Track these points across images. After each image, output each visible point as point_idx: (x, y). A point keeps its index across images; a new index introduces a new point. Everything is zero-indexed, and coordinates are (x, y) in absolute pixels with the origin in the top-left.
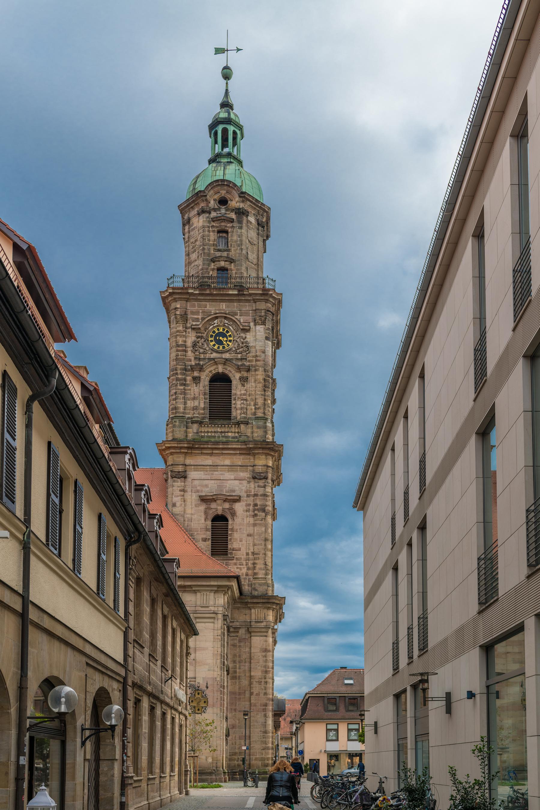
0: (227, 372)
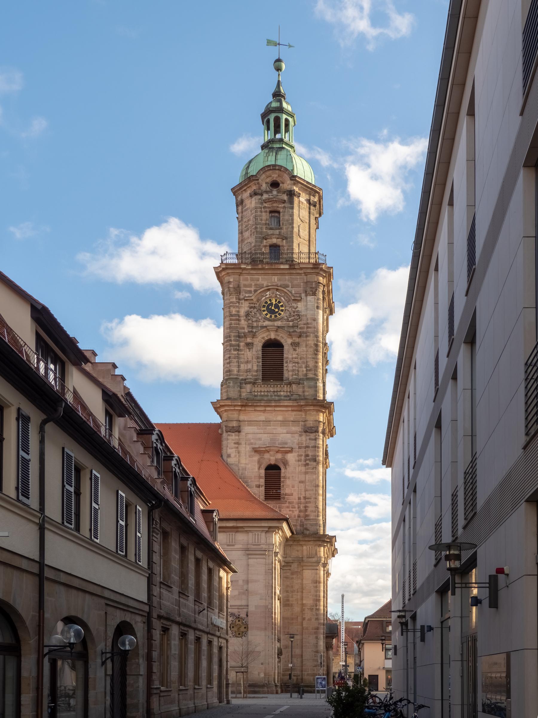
0: (279, 338)
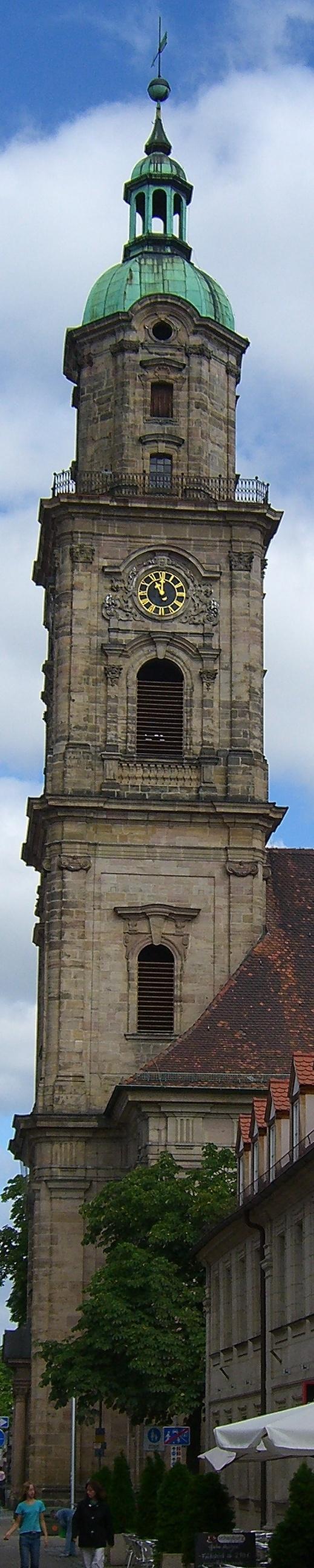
0: (169, 657)
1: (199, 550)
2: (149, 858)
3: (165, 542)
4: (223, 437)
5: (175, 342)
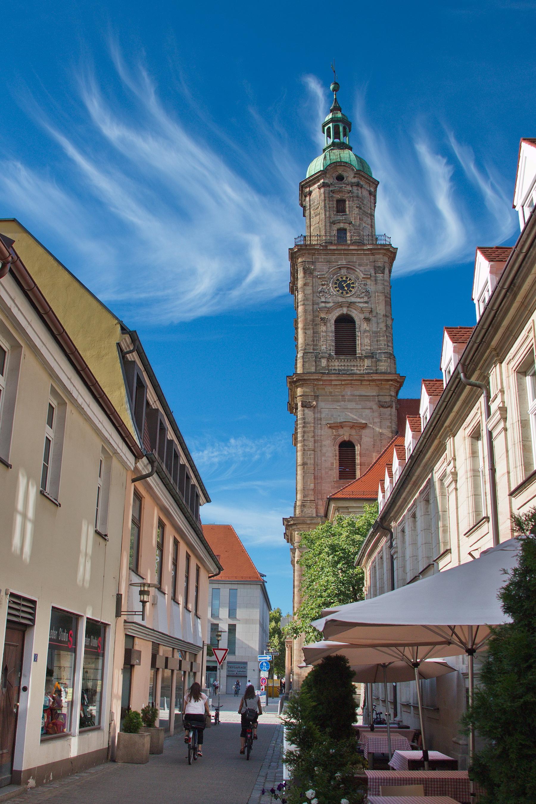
0: (349, 313)
1: (360, 266)
2: (342, 401)
3: (345, 263)
4: (369, 221)
5: (346, 182)
